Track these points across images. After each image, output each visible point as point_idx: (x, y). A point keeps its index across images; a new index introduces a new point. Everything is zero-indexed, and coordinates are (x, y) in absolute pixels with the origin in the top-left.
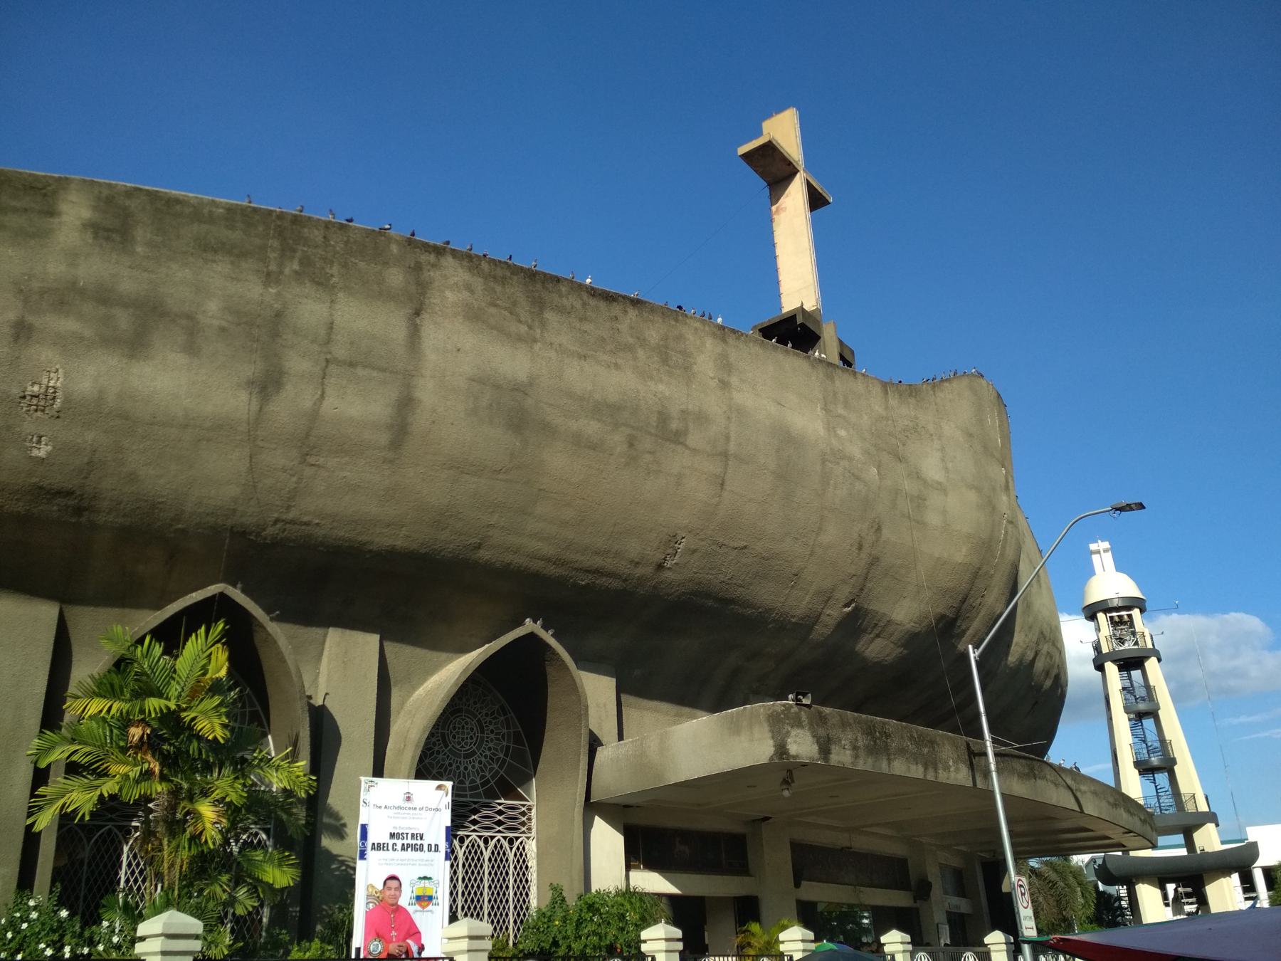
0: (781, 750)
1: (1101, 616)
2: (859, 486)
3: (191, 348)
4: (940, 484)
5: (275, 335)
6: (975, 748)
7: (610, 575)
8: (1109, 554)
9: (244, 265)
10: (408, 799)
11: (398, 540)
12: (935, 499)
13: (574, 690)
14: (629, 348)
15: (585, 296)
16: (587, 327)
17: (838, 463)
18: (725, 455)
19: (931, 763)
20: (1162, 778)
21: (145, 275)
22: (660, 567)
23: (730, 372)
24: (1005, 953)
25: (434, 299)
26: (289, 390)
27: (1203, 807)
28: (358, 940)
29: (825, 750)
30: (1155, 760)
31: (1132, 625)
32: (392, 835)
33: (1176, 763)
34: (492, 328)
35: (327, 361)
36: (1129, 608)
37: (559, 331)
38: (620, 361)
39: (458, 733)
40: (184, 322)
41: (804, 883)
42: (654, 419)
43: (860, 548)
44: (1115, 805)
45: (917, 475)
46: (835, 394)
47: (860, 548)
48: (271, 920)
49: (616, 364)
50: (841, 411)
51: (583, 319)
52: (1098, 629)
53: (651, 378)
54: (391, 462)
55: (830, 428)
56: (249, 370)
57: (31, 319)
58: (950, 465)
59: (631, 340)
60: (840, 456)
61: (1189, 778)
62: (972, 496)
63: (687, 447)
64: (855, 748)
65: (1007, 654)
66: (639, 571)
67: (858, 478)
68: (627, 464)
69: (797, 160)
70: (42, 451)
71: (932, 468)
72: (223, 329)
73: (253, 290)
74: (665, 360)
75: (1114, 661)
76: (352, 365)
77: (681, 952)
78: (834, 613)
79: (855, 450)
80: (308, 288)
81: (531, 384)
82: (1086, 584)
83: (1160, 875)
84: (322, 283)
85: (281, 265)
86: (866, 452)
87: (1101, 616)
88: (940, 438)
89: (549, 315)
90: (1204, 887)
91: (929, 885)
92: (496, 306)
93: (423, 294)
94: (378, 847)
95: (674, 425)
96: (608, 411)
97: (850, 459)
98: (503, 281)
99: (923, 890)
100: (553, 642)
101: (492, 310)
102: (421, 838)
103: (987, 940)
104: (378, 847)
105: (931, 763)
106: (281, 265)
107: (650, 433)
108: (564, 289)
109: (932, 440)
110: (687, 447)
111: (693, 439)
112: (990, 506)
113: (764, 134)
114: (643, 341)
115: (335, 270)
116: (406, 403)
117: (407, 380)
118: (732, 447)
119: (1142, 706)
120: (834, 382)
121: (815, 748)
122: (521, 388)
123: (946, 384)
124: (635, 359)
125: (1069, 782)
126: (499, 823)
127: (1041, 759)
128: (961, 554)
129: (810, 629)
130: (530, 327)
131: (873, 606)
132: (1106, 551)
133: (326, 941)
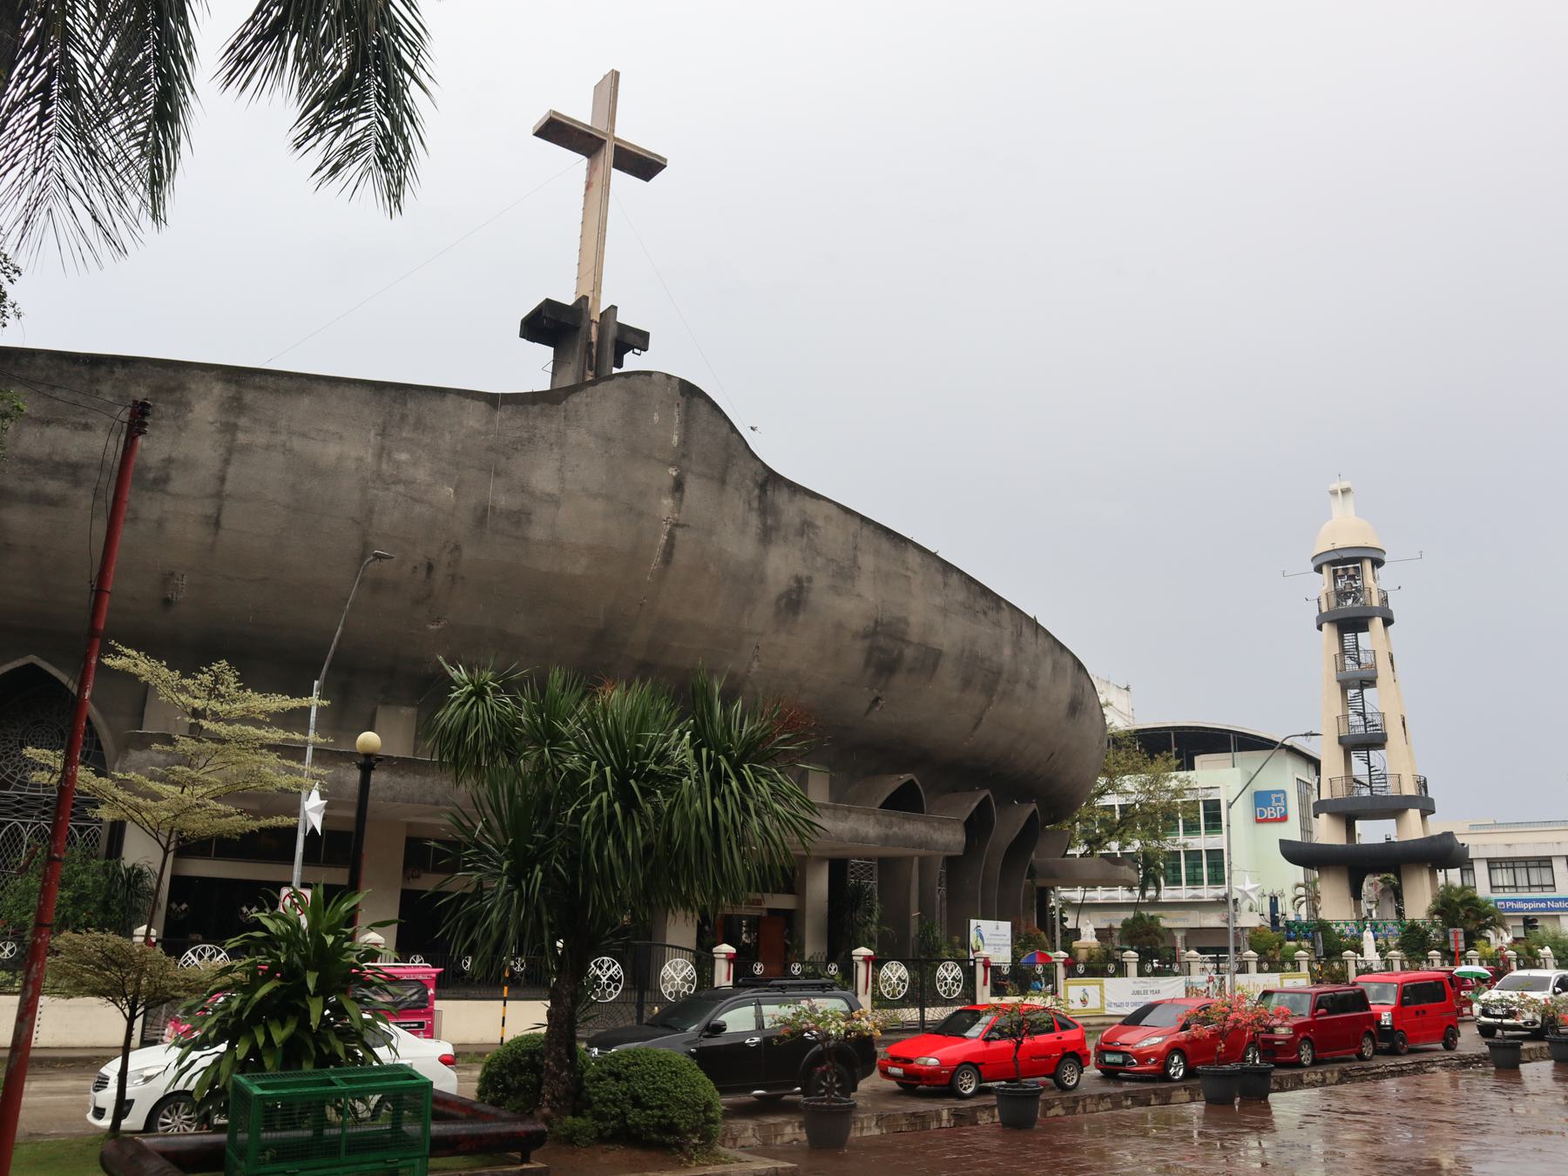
13: (364, 744)
39: (37, 740)
45: (524, 489)
48: (507, 869)
58: (568, 475)
102: (1217, 878)
109: (551, 450)
126: (17, 811)
127: (354, 836)
133: (428, 883)
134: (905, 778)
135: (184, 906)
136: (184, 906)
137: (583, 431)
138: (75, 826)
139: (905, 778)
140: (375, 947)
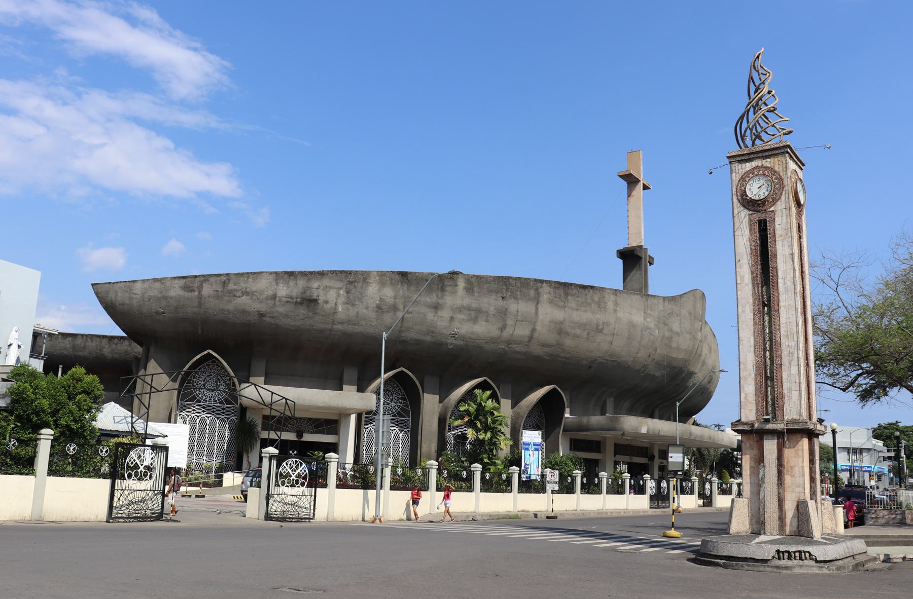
2: (652, 337)
3: (487, 321)
4: (678, 332)
5: (505, 315)
9: (498, 295)
12: (675, 338)
14: (590, 304)
16: (579, 299)
17: (646, 331)
18: (613, 334)
21: (477, 301)
23: (617, 307)
25: (541, 299)
26: (507, 329)
34: (555, 305)
35: (517, 321)
37: (572, 302)
38: (587, 309)
40: (486, 313)
42: (595, 327)
45: (671, 330)
46: (648, 305)
49: (586, 311)
53: (595, 313)
54: (527, 345)
55: (645, 319)
56: (500, 325)
57: (454, 316)
58: (682, 325)
59: (590, 301)
60: (647, 328)
67: (652, 335)
68: (586, 341)
72: (494, 315)
73: (501, 303)
74: (599, 307)
76: (522, 321)
77: (52, 440)
79: (652, 325)
80: (513, 300)
81: (564, 321)
84: (516, 298)
85: (506, 294)
86: (656, 325)
88: (680, 316)
89: (570, 298)
92: (556, 297)
93: (539, 297)
95: (600, 327)
96: (582, 326)
97: (650, 329)
98: (557, 288)
101: (555, 299)
106: (506, 294)
107: (593, 331)
108: (573, 287)
111: (605, 331)
113: (868, 547)
114: (593, 301)
115: (518, 293)
116: (534, 330)
117: (534, 323)
118: (615, 332)
120: (648, 301)
122: (561, 323)
124: (591, 307)
130: (564, 303)
134: (548, 388)
135: (295, 452)
136: (295, 452)
137: (685, 310)
138: (225, 418)
139: (548, 388)
140: (783, 430)
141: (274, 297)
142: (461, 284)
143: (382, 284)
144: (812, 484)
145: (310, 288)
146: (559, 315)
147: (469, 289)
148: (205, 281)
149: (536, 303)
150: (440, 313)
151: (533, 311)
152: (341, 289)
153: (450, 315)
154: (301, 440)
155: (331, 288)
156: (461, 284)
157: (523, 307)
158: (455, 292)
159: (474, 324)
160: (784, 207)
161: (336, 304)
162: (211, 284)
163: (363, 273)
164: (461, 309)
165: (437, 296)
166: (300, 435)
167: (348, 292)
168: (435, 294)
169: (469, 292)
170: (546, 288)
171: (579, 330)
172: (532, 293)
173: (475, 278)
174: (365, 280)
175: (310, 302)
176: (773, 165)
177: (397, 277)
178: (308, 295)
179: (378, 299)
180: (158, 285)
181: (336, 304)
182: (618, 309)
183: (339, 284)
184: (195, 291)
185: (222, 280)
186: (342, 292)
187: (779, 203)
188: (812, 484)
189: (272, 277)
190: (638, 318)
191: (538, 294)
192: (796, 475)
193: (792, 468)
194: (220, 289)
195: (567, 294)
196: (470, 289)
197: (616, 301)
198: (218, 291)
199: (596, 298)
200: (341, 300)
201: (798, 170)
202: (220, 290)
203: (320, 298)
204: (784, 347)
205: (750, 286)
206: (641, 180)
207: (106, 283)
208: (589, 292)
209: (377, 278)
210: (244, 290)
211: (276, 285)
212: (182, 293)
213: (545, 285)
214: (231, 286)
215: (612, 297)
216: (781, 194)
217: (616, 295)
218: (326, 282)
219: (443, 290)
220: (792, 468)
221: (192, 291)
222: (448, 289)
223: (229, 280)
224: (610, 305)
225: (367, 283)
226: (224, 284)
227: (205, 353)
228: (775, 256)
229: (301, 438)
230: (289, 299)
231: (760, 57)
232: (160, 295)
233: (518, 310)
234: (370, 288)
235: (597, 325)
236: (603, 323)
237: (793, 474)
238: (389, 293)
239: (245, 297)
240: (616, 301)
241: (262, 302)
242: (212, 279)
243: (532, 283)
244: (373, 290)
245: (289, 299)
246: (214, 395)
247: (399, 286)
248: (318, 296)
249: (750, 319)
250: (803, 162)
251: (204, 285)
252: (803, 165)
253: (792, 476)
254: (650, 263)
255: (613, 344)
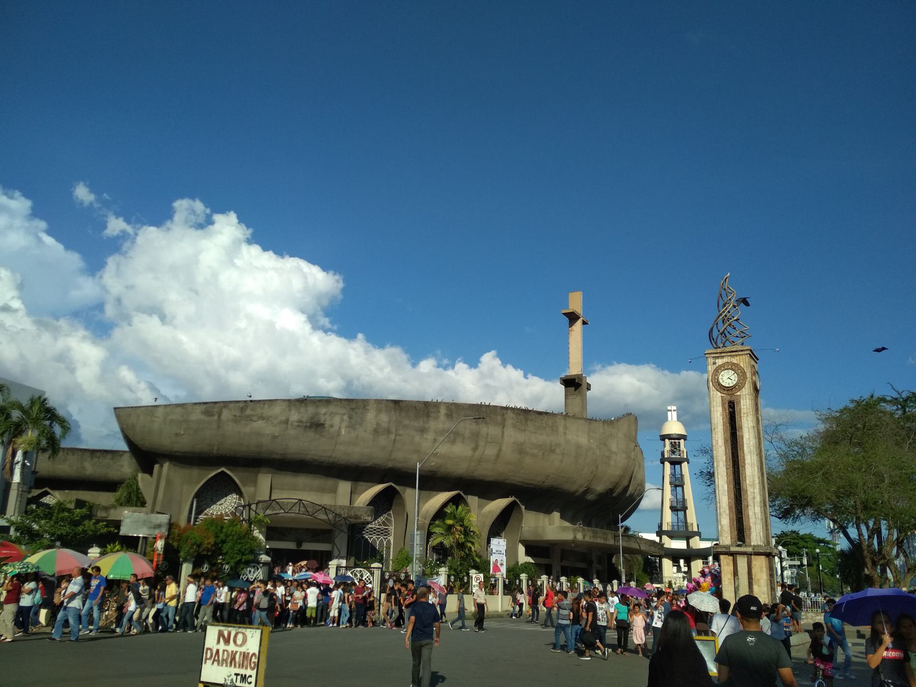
0: (575, 537)
1: (667, 441)
3: (463, 442)
5: (478, 437)
6: (616, 535)
7: (533, 485)
8: (675, 412)
10: (499, 543)
11: (491, 479)
14: (545, 428)
15: (536, 414)
18: (564, 454)
19: (606, 539)
20: (681, 514)
22: (544, 482)
24: (792, 644)
27: (695, 529)
28: (491, 572)
29: (584, 537)
30: (679, 507)
31: (679, 447)
32: (497, 551)
33: (687, 509)
36: (679, 439)
41: (564, 561)
43: (592, 473)
44: (650, 546)
47: (592, 473)
50: (592, 434)
51: (536, 422)
52: (665, 446)
55: (589, 440)
59: (545, 426)
61: (692, 517)
62: (624, 455)
63: (555, 453)
64: (590, 537)
65: (626, 493)
66: (539, 483)
69: (580, 313)
70: (433, 464)
71: (614, 447)
73: (474, 427)
75: (669, 462)
76: (491, 442)
78: (582, 490)
79: (594, 446)
82: (662, 425)
83: (675, 556)
87: (667, 441)
89: (529, 422)
90: (691, 562)
91: (593, 562)
94: (494, 553)
95: (553, 448)
98: (519, 414)
99: (590, 563)
100: (519, 502)
103: (613, 582)
104: (494, 553)
105: (606, 539)
110: (555, 453)
111: (558, 451)
112: (629, 457)
116: (500, 450)
119: (677, 483)
121: (582, 537)
123: (621, 420)
125: (638, 541)
128: (618, 472)
129: (575, 493)
131: (592, 487)
132: (674, 411)
141: (287, 422)
142: (443, 411)
143: (379, 411)
144: (773, 592)
145: (317, 414)
146: (521, 437)
147: (449, 415)
148: (225, 407)
149: (502, 427)
150: (425, 436)
151: (500, 434)
152: (344, 414)
153: (433, 437)
154: (300, 549)
155: (336, 414)
156: (443, 411)
157: (492, 430)
158: (437, 418)
159: (453, 445)
160: (747, 393)
161: (340, 428)
162: (231, 410)
163: (363, 400)
164: (442, 432)
165: (423, 421)
166: (299, 544)
167: (350, 417)
168: (421, 420)
169: (449, 417)
170: (510, 414)
171: (536, 451)
172: (499, 418)
173: (454, 405)
174: (364, 406)
175: (316, 425)
176: (739, 362)
177: (392, 405)
178: (316, 420)
179: (375, 424)
180: (179, 410)
181: (340, 428)
182: (567, 432)
183: (343, 411)
184: (215, 415)
185: (241, 406)
186: (345, 417)
187: (743, 389)
188: (773, 592)
189: (285, 405)
190: (583, 440)
191: (504, 420)
192: (762, 585)
193: (758, 580)
194: (238, 413)
195: (526, 420)
196: (449, 415)
197: (565, 425)
198: (236, 416)
199: (550, 423)
200: (344, 425)
201: (755, 364)
202: (238, 415)
203: (327, 422)
204: (749, 493)
205: (723, 447)
206: (581, 317)
207: (128, 407)
208: (544, 417)
209: (375, 406)
210: (260, 415)
211: (289, 411)
212: (202, 417)
213: (509, 411)
214: (248, 412)
215: (563, 422)
216: (745, 383)
217: (566, 420)
218: (332, 408)
219: (428, 416)
220: (758, 580)
221: (212, 415)
222: (432, 414)
223: (247, 406)
224: (561, 429)
225: (366, 409)
226: (242, 410)
227: (220, 471)
228: (741, 428)
229: (301, 547)
230: (300, 424)
231: (727, 280)
232: (181, 419)
233: (488, 434)
234: (369, 414)
235: (551, 446)
236: (556, 444)
237: (759, 584)
238: (384, 418)
239: (260, 421)
240: (565, 425)
241: (275, 426)
242: (231, 405)
243: (499, 410)
244: (371, 416)
245: (300, 424)
246: (221, 508)
247: (393, 413)
248: (325, 421)
249: (724, 471)
250: (758, 357)
251: (224, 410)
252: (758, 359)
253: (759, 586)
254: (587, 389)
255: (563, 462)
